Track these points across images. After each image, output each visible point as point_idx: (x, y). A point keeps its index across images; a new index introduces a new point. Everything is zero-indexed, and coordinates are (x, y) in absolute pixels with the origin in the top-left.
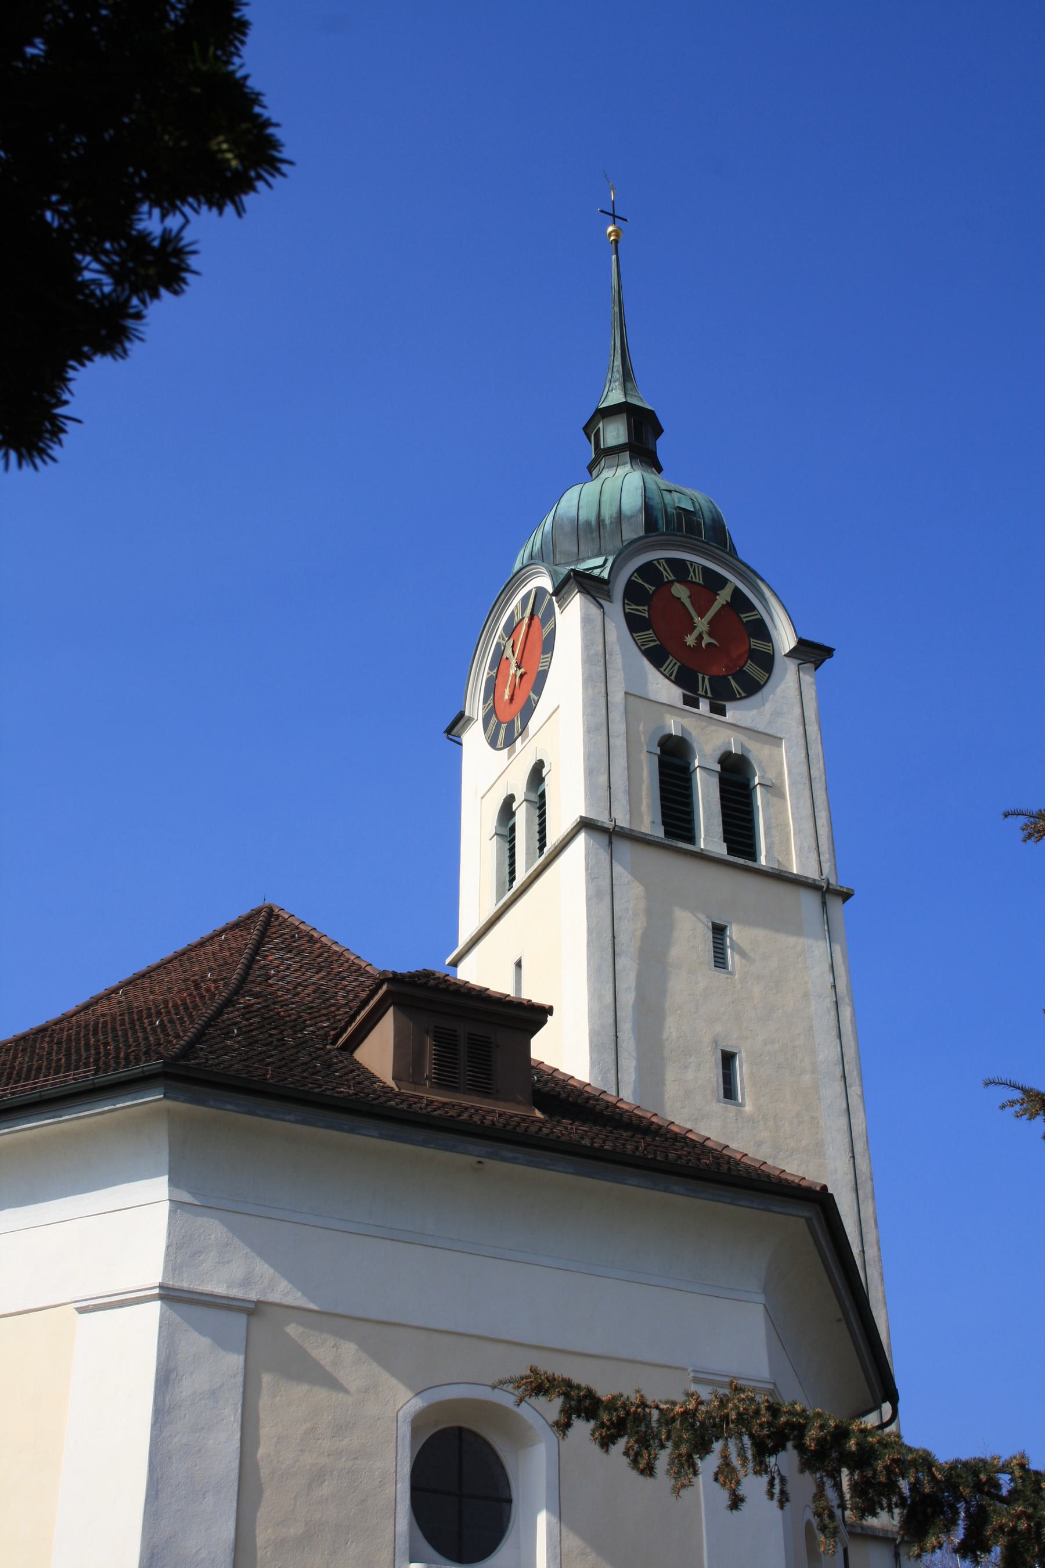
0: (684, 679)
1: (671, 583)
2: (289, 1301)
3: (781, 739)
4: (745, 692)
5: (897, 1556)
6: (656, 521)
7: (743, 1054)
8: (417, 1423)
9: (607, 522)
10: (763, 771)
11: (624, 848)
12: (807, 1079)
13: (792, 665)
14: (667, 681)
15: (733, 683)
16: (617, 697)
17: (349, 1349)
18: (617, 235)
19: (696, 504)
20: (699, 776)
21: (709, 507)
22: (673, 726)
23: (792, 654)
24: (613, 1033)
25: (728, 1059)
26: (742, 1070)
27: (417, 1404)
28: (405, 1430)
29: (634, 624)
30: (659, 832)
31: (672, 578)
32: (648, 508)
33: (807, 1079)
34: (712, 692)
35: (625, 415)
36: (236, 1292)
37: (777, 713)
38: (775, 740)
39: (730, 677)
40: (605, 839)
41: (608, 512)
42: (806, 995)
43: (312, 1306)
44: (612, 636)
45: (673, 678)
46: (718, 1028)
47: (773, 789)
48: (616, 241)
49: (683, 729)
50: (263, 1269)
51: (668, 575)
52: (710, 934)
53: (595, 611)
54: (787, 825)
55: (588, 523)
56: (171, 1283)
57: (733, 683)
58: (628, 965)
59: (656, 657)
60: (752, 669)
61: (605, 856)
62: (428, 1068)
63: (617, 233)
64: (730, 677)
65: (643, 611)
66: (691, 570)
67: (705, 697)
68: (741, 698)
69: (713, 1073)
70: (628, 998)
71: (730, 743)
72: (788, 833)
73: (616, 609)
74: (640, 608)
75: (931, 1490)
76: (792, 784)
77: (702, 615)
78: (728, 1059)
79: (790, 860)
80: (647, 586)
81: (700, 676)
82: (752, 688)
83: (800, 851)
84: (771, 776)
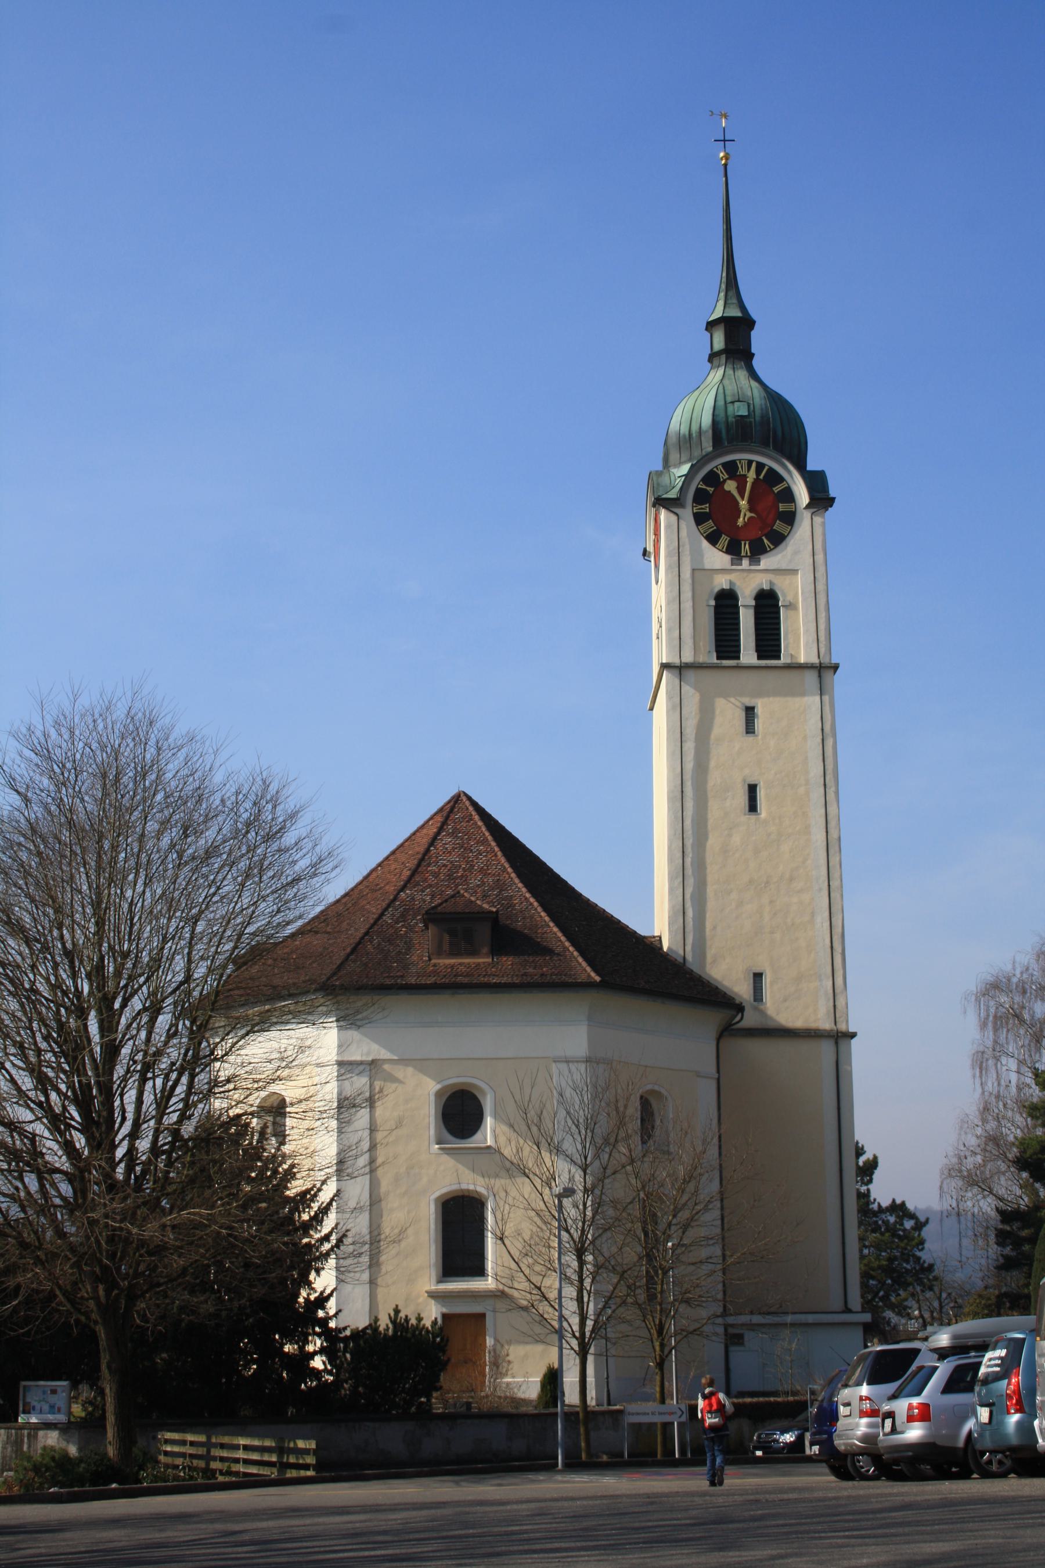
0: (733, 550)
1: (725, 481)
2: (385, 1057)
3: (798, 570)
4: (773, 544)
5: (837, 1043)
6: (721, 432)
7: (762, 783)
8: (438, 1094)
9: (694, 435)
10: (784, 596)
11: (690, 675)
12: (802, 790)
13: (807, 514)
14: (721, 553)
15: (766, 541)
16: (687, 574)
17: (410, 1070)
18: (727, 159)
19: (752, 406)
20: (742, 611)
21: (761, 405)
22: (722, 582)
23: (808, 507)
24: (680, 790)
25: (752, 789)
26: (761, 794)
27: (439, 1086)
28: (432, 1098)
29: (699, 519)
30: (714, 660)
31: (727, 476)
32: (715, 423)
33: (802, 790)
34: (751, 552)
35: (723, 324)
36: (364, 1058)
37: (796, 553)
38: (794, 572)
39: (764, 538)
40: (677, 671)
41: (695, 428)
42: (805, 738)
43: (396, 1058)
44: (684, 533)
45: (724, 550)
46: (747, 771)
47: (792, 606)
48: (726, 165)
49: (731, 582)
50: (375, 1047)
51: (723, 475)
52: (743, 714)
53: (674, 518)
54: (799, 629)
55: (684, 435)
56: (340, 1059)
57: (766, 541)
58: (690, 746)
59: (713, 539)
60: (778, 526)
61: (677, 681)
62: (446, 947)
63: (727, 157)
64: (764, 538)
65: (706, 508)
66: (740, 466)
67: (746, 556)
68: (771, 550)
69: (742, 799)
70: (689, 765)
71: (762, 583)
72: (799, 635)
73: (687, 513)
74: (703, 507)
75: (216, 1308)
76: (804, 600)
77: (743, 499)
78: (752, 789)
79: (799, 653)
80: (708, 489)
81: (743, 543)
82: (778, 539)
83: (806, 645)
84: (790, 598)
